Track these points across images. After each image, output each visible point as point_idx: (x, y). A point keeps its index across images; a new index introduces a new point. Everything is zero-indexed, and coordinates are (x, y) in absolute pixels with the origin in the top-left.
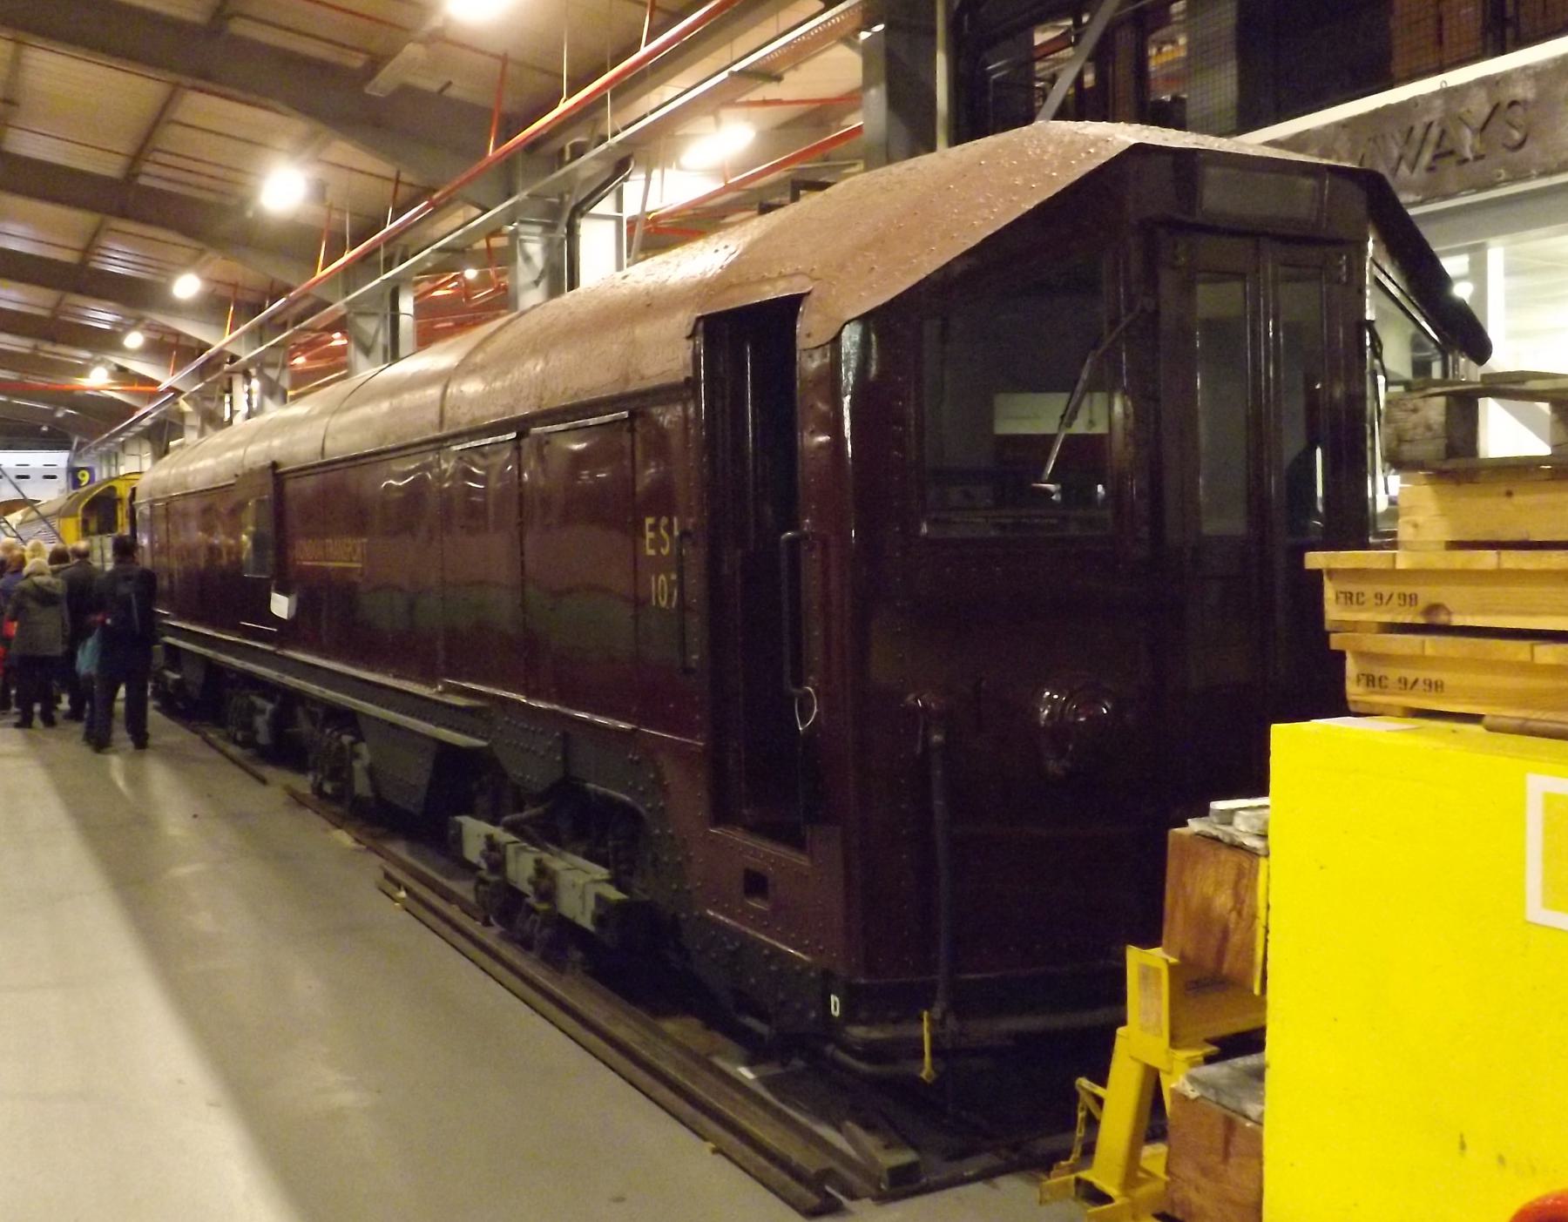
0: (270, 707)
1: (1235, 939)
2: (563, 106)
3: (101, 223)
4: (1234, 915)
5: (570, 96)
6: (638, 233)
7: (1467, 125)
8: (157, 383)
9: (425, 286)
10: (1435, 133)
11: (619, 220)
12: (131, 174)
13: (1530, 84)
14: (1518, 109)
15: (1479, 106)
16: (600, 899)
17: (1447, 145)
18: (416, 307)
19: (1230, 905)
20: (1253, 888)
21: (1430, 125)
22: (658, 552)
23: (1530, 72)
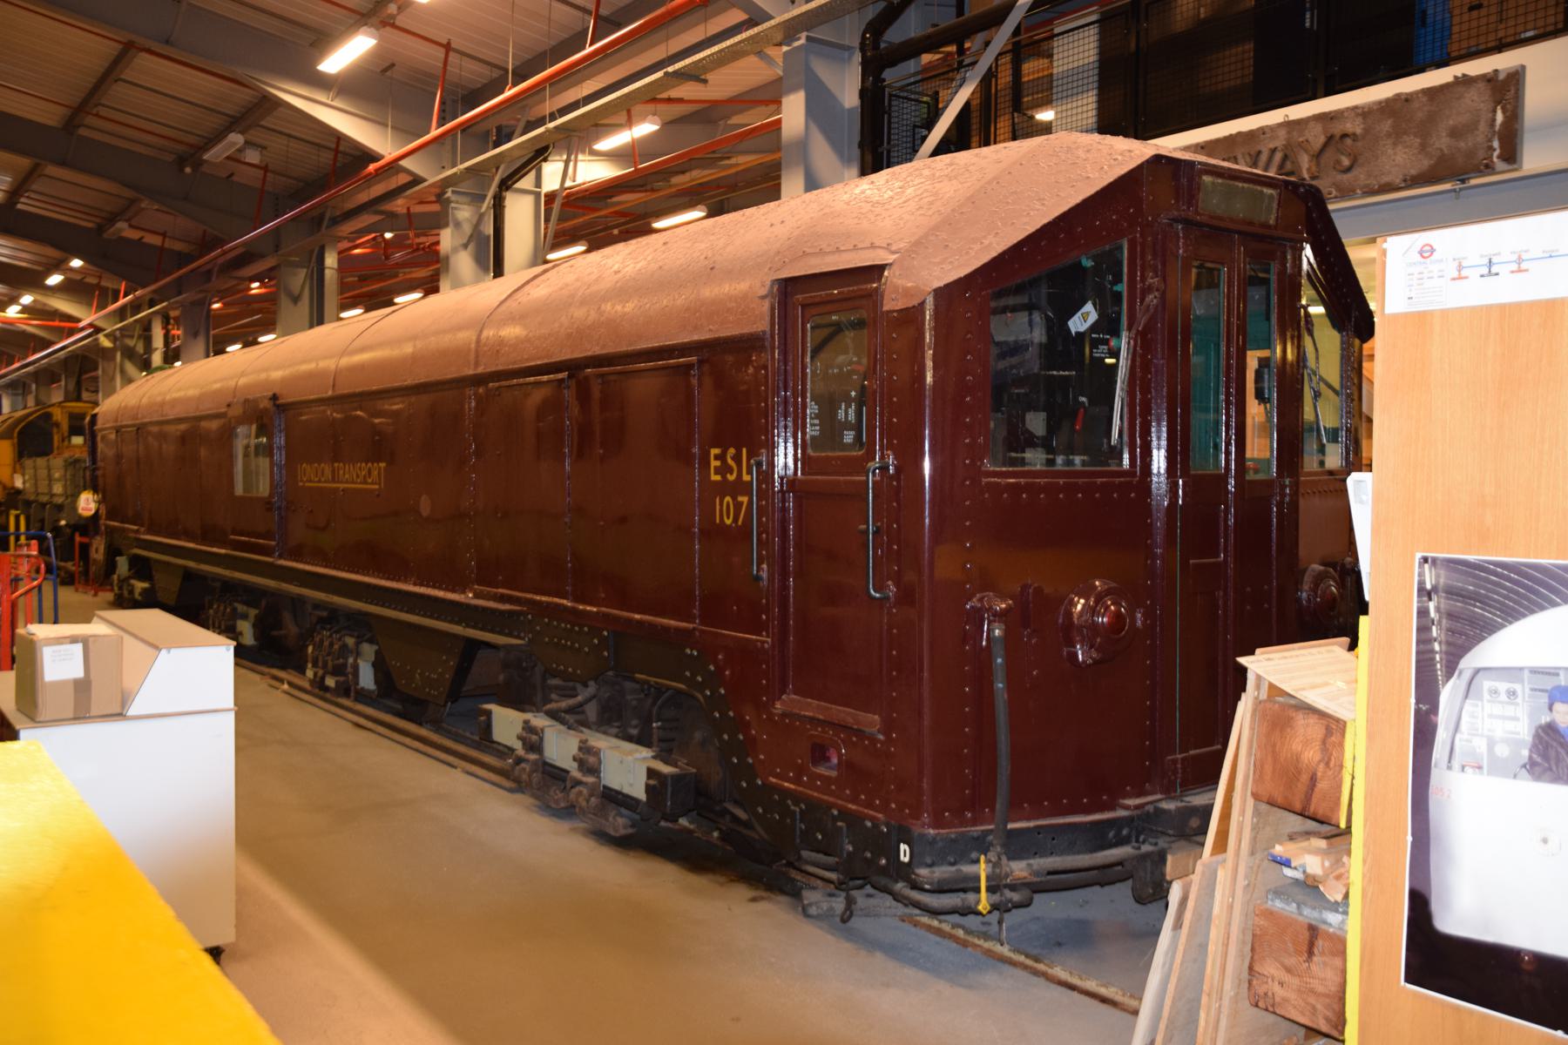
0: (253, 612)
1: (1322, 785)
3: (36, 167)
4: (1322, 766)
5: (514, 85)
6: (556, 206)
7: (1306, 151)
8: (79, 320)
9: (345, 245)
10: (1278, 156)
11: (538, 195)
12: (71, 124)
13: (1359, 120)
14: (1349, 141)
15: (1317, 138)
16: (651, 773)
17: (1289, 166)
18: (339, 261)
19: (1318, 757)
20: (1341, 745)
21: (1273, 151)
22: (724, 477)
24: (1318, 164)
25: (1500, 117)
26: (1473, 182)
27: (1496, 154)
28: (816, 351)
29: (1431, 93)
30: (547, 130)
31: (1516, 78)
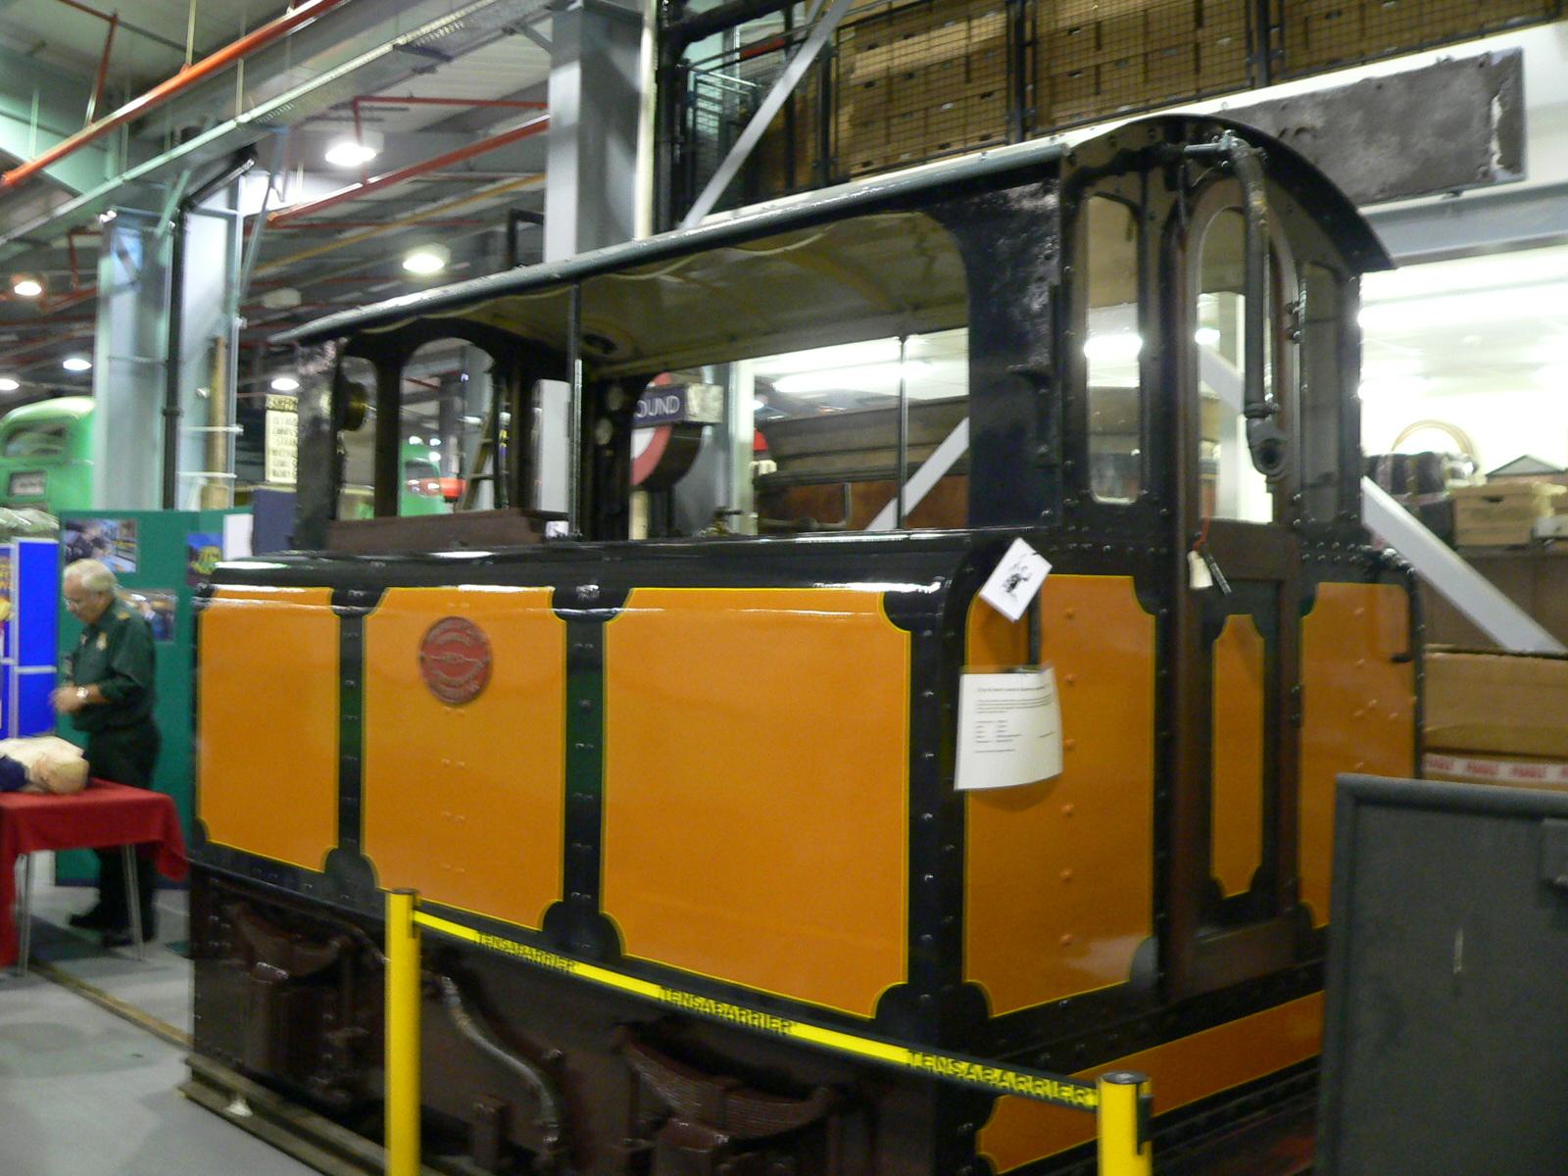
2: (185, 74)
11: (231, 220)
23: (1319, 99)
24: (838, 37)
25: (1497, 111)
26: (1467, 194)
27: (1496, 157)
28: (75, 194)
29: (1410, 78)
30: (239, 125)
31: (1514, 62)
